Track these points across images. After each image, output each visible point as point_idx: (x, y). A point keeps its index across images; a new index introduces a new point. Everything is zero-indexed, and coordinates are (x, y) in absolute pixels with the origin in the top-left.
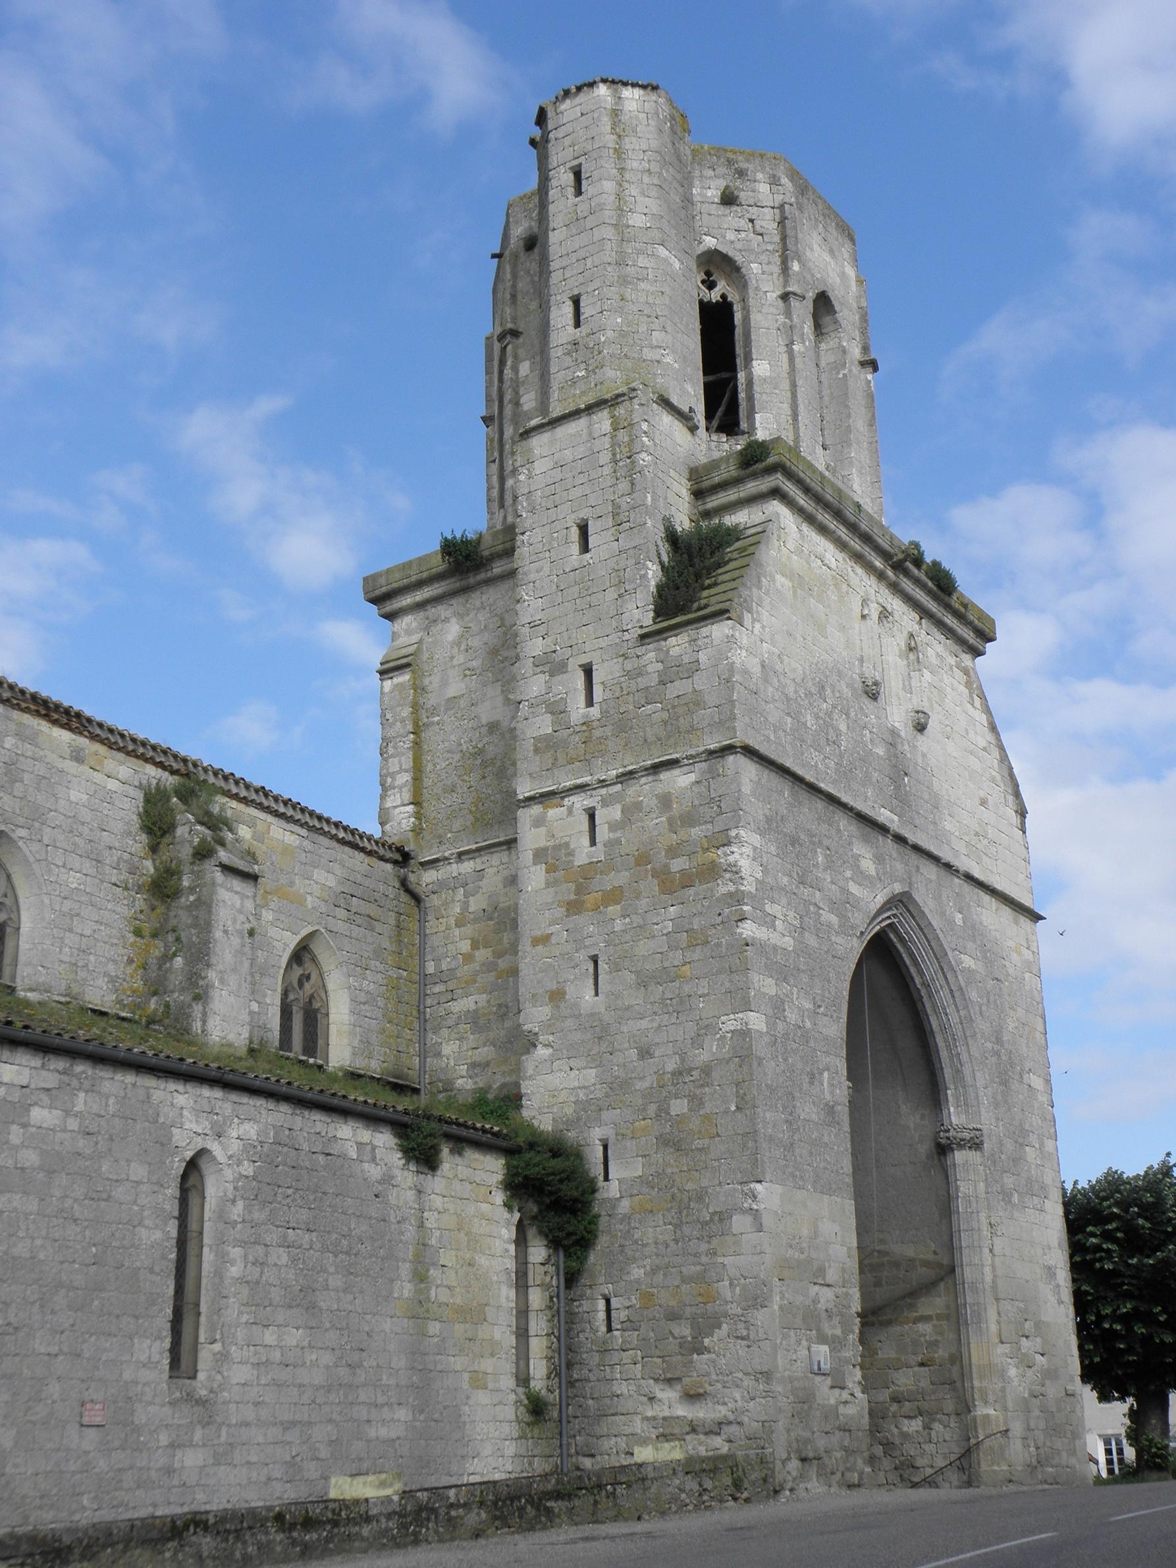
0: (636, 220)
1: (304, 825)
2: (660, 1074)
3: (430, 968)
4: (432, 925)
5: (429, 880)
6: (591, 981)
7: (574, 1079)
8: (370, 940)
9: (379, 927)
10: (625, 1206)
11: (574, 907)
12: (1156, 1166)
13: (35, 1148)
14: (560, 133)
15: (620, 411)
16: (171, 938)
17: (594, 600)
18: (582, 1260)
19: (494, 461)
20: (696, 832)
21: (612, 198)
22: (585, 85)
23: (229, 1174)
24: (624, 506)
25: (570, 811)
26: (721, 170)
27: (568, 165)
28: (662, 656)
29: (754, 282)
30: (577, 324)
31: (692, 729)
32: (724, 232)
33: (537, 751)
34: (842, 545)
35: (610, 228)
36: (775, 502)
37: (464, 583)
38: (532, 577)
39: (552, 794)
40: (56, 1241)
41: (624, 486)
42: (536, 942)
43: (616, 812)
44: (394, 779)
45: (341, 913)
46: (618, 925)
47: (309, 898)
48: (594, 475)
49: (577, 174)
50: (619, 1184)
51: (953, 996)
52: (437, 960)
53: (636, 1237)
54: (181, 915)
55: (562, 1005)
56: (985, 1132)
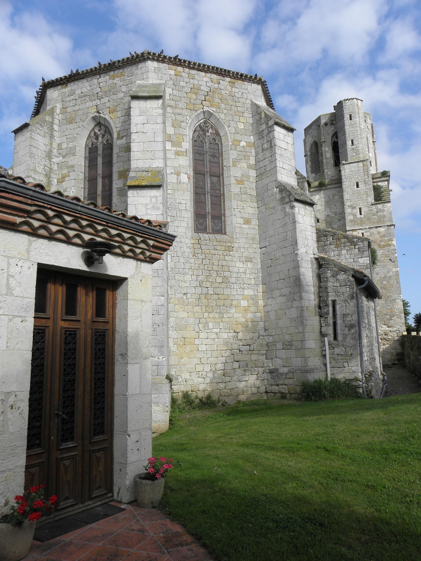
0: (362, 127)
2: (381, 277)
14: (346, 107)
15: (365, 163)
33: (350, 222)
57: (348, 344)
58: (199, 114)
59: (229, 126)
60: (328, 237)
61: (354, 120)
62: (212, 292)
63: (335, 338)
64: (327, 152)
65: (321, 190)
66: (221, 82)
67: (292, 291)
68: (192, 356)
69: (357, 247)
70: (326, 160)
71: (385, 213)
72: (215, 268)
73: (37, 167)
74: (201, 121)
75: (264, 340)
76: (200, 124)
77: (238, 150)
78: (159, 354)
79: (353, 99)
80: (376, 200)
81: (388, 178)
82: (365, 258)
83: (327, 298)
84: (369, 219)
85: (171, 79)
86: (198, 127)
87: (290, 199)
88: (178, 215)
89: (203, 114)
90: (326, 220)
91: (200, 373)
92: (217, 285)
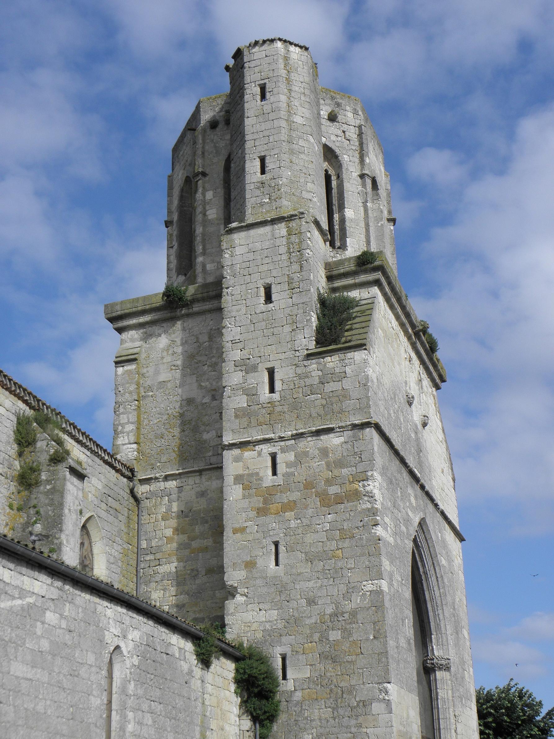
0: (298, 119)
1: (89, 449)
2: (322, 615)
3: (144, 544)
4: (145, 518)
5: (144, 491)
6: (273, 557)
7: (262, 616)
8: (116, 524)
9: (121, 517)
10: (298, 696)
11: (262, 512)
12: (502, 687)
13: (47, 638)
14: (252, 64)
15: (293, 224)
16: (32, 511)
17: (276, 331)
18: (269, 729)
19: (172, 247)
20: (345, 471)
21: (285, 105)
22: (268, 40)
23: (128, 663)
24: (296, 279)
25: (260, 454)
26: (328, 101)
27: (257, 83)
28: (321, 367)
29: (345, 165)
30: (263, 172)
31: (341, 411)
32: (332, 135)
33: (236, 416)
34: (398, 318)
35: (284, 121)
36: (376, 288)
37: (173, 314)
38: (234, 314)
39: (247, 443)
40: (56, 702)
41: (296, 267)
42: (235, 531)
43: (291, 456)
44: (123, 427)
45: (103, 506)
46: (293, 524)
47: (90, 495)
48: (275, 259)
49: (263, 89)
50: (293, 683)
51: (437, 581)
52: (149, 540)
53: (306, 715)
54: (40, 496)
55: (254, 571)
56: (452, 661)
61: (272, 99)
65: (173, 319)
70: (204, 226)
71: (347, 384)
79: (272, 41)
84: (295, 406)
90: (182, 415)
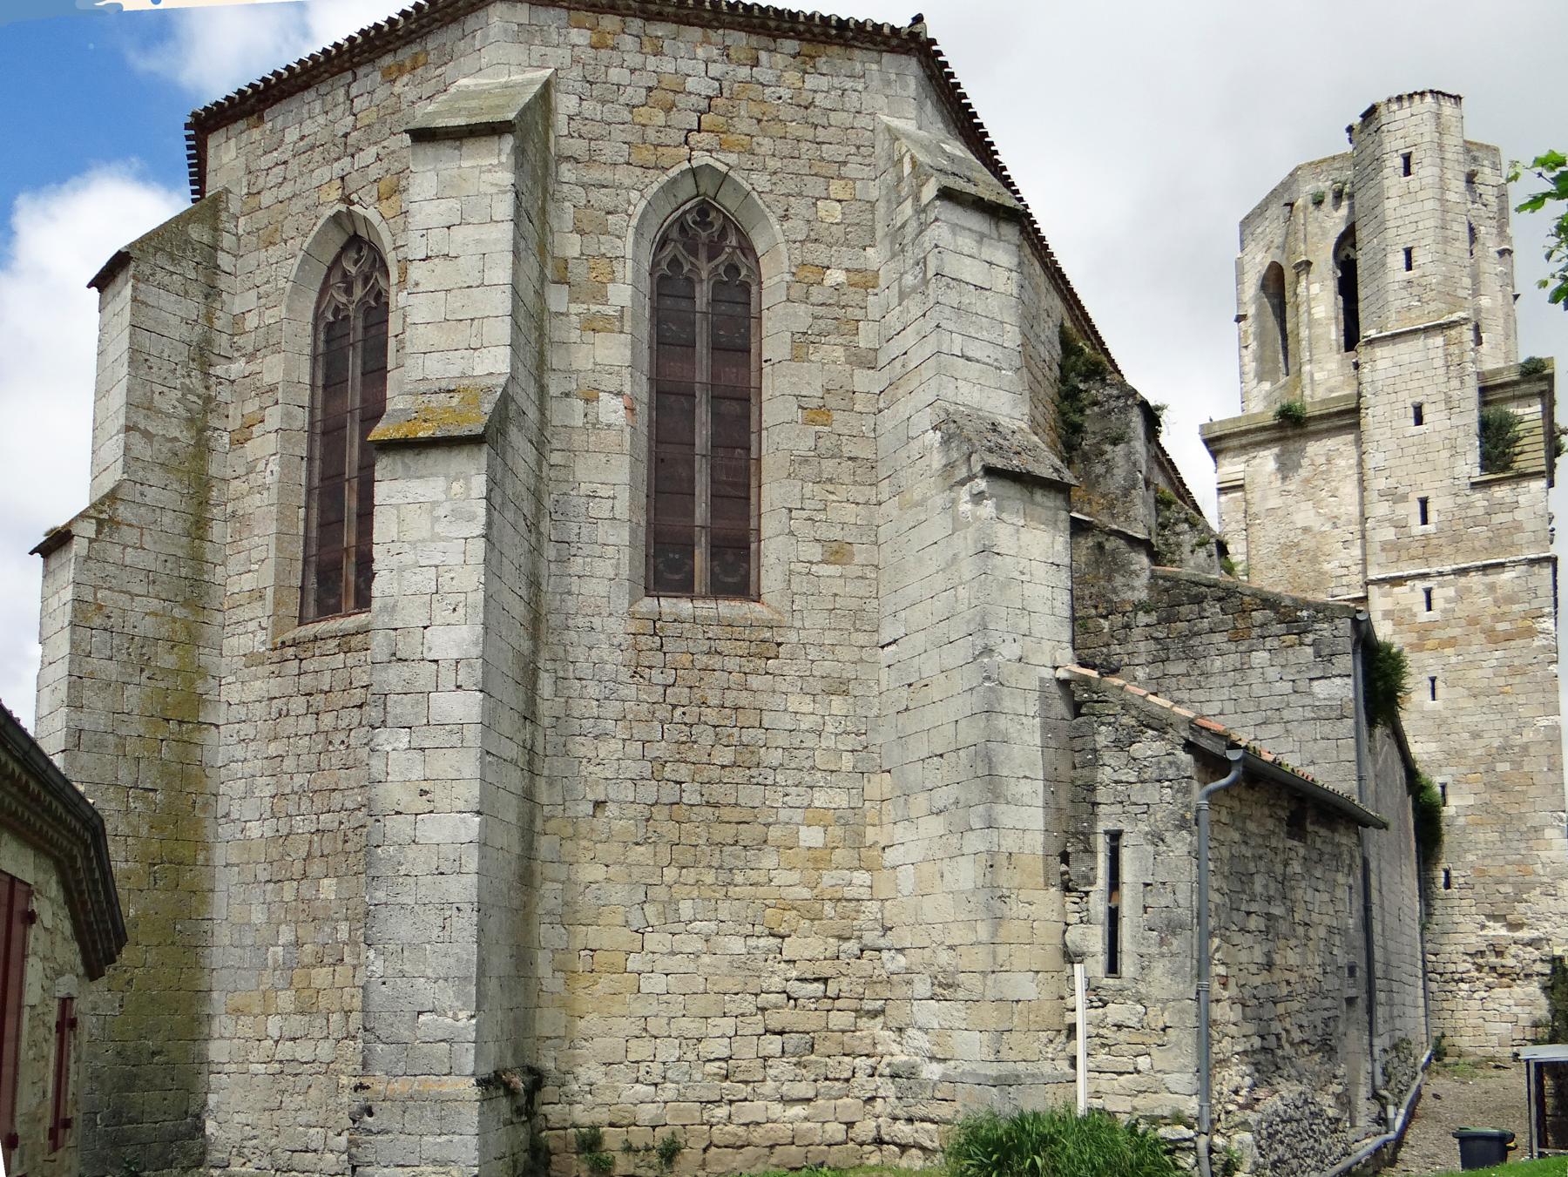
14: (1392, 127)
33: (1383, 550)
57: (1155, 992)
58: (673, 182)
59: (785, 217)
60: (1205, 605)
62: (696, 799)
63: (1113, 968)
64: (1318, 299)
66: (763, 56)
67: (962, 799)
68: (616, 1009)
69: (1309, 638)
71: (1519, 515)
72: (711, 715)
73: (156, 396)
74: (688, 206)
75: (877, 963)
76: (685, 212)
77: (812, 299)
78: (459, 1004)
80: (1487, 462)
81: (1544, 386)
82: (1338, 681)
83: (1092, 825)
84: (1456, 540)
85: (575, 61)
86: (676, 228)
87: (970, 469)
88: (584, 538)
89: (690, 181)
91: (643, 1067)
92: (716, 773)
